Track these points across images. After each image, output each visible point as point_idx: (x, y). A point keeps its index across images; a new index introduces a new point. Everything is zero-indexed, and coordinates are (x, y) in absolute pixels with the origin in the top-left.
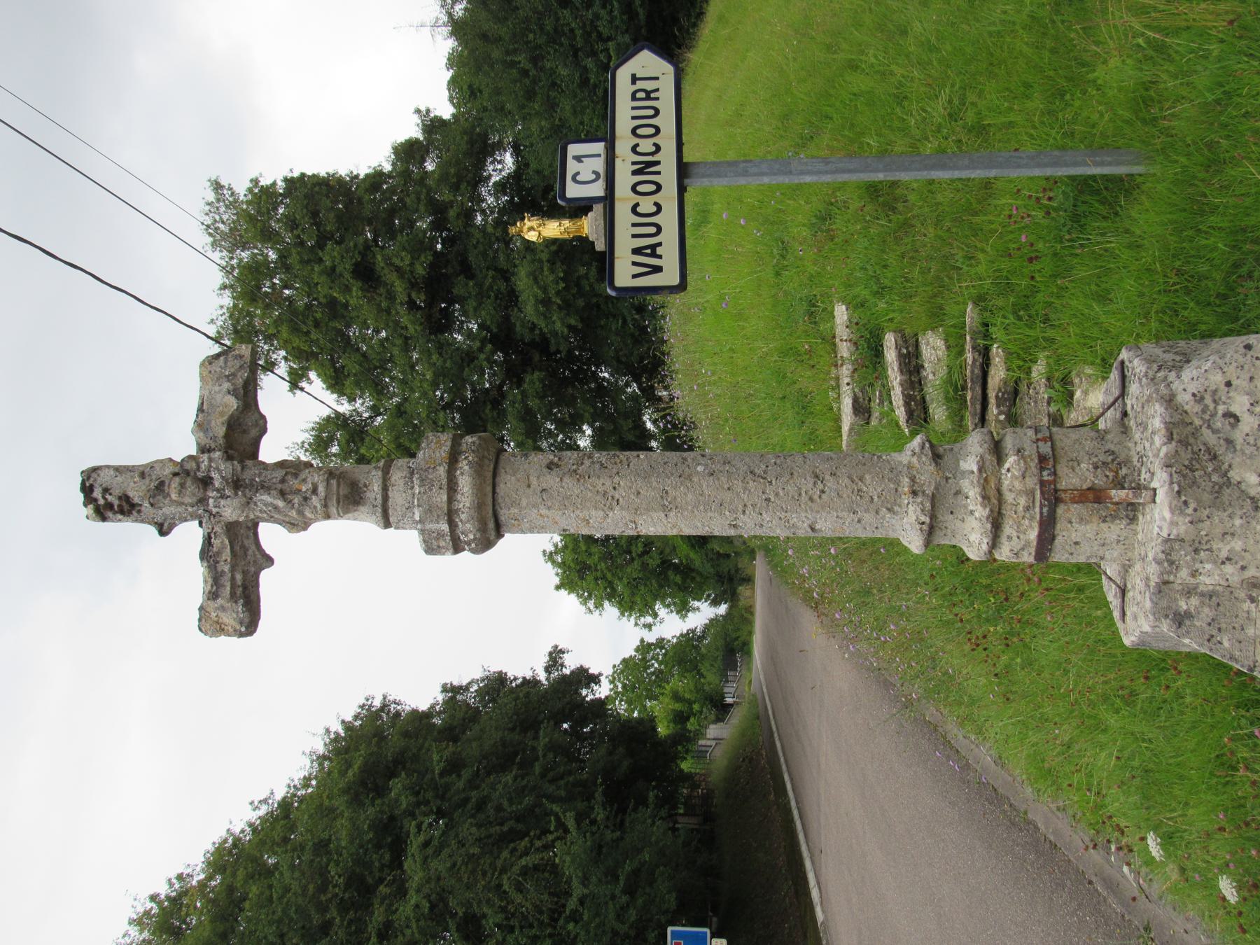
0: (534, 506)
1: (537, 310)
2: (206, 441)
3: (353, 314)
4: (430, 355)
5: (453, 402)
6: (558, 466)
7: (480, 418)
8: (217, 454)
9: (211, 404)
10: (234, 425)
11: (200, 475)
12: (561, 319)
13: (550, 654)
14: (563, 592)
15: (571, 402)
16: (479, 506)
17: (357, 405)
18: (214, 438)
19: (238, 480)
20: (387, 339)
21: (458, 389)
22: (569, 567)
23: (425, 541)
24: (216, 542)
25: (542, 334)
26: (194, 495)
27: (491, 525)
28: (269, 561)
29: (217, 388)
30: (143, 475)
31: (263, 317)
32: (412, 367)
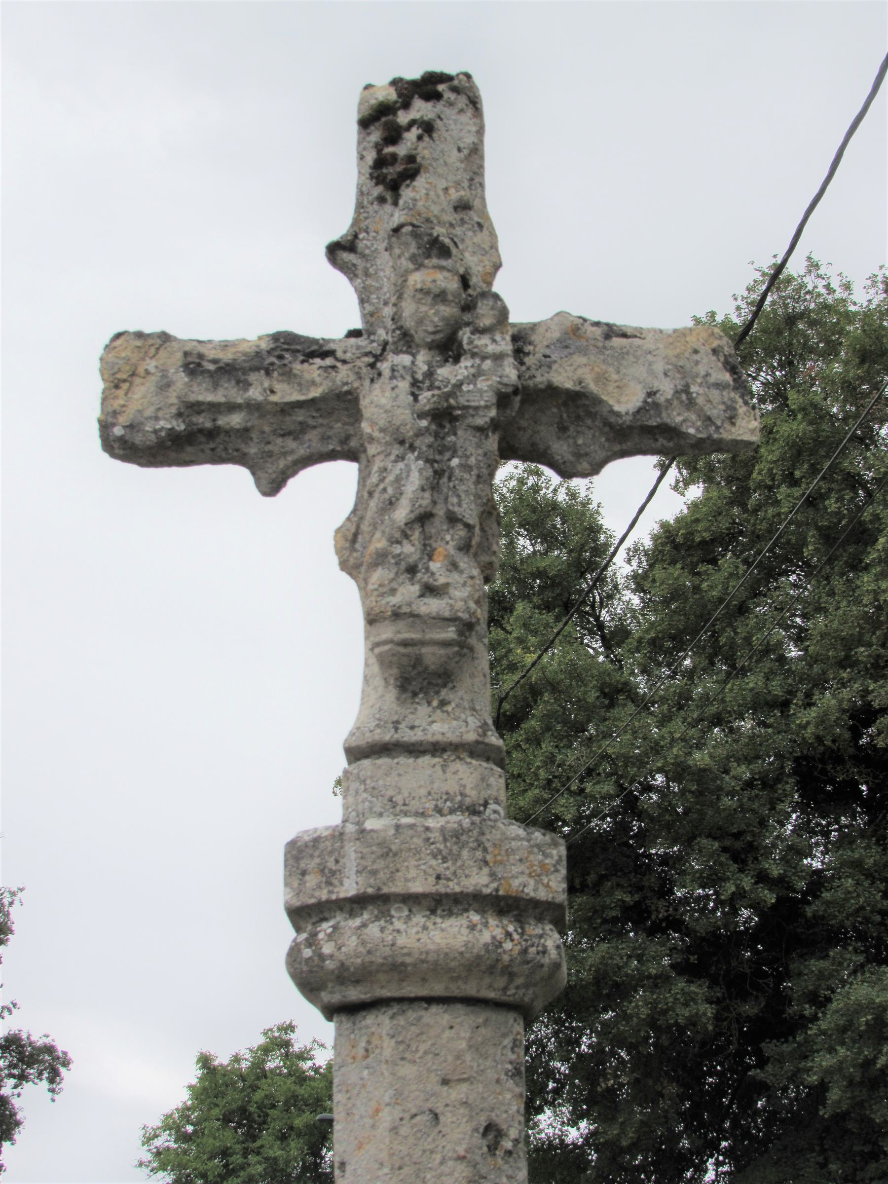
0: (398, 1094)
1: (859, 1009)
2: (540, 345)
3: (838, 583)
4: (748, 760)
5: (640, 815)
6: (492, 1148)
7: (602, 878)
8: (510, 372)
9: (623, 354)
10: (577, 405)
11: (465, 335)
12: (840, 1068)
13: (49, 1049)
14: (193, 1074)
15: (644, 1093)
16: (396, 968)
17: (628, 595)
18: (547, 363)
19: (454, 419)
20: (782, 659)
21: (669, 826)
22: (254, 1088)
23: (317, 840)
24: (313, 370)
25: (803, 1022)
26: (420, 322)
27: (354, 994)
28: (272, 486)
29: (659, 367)
30: (463, 207)
31: (827, 380)
32: (717, 720)
